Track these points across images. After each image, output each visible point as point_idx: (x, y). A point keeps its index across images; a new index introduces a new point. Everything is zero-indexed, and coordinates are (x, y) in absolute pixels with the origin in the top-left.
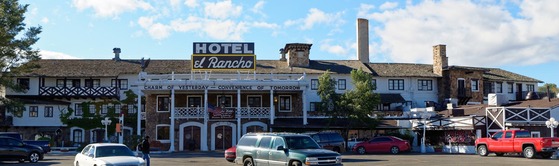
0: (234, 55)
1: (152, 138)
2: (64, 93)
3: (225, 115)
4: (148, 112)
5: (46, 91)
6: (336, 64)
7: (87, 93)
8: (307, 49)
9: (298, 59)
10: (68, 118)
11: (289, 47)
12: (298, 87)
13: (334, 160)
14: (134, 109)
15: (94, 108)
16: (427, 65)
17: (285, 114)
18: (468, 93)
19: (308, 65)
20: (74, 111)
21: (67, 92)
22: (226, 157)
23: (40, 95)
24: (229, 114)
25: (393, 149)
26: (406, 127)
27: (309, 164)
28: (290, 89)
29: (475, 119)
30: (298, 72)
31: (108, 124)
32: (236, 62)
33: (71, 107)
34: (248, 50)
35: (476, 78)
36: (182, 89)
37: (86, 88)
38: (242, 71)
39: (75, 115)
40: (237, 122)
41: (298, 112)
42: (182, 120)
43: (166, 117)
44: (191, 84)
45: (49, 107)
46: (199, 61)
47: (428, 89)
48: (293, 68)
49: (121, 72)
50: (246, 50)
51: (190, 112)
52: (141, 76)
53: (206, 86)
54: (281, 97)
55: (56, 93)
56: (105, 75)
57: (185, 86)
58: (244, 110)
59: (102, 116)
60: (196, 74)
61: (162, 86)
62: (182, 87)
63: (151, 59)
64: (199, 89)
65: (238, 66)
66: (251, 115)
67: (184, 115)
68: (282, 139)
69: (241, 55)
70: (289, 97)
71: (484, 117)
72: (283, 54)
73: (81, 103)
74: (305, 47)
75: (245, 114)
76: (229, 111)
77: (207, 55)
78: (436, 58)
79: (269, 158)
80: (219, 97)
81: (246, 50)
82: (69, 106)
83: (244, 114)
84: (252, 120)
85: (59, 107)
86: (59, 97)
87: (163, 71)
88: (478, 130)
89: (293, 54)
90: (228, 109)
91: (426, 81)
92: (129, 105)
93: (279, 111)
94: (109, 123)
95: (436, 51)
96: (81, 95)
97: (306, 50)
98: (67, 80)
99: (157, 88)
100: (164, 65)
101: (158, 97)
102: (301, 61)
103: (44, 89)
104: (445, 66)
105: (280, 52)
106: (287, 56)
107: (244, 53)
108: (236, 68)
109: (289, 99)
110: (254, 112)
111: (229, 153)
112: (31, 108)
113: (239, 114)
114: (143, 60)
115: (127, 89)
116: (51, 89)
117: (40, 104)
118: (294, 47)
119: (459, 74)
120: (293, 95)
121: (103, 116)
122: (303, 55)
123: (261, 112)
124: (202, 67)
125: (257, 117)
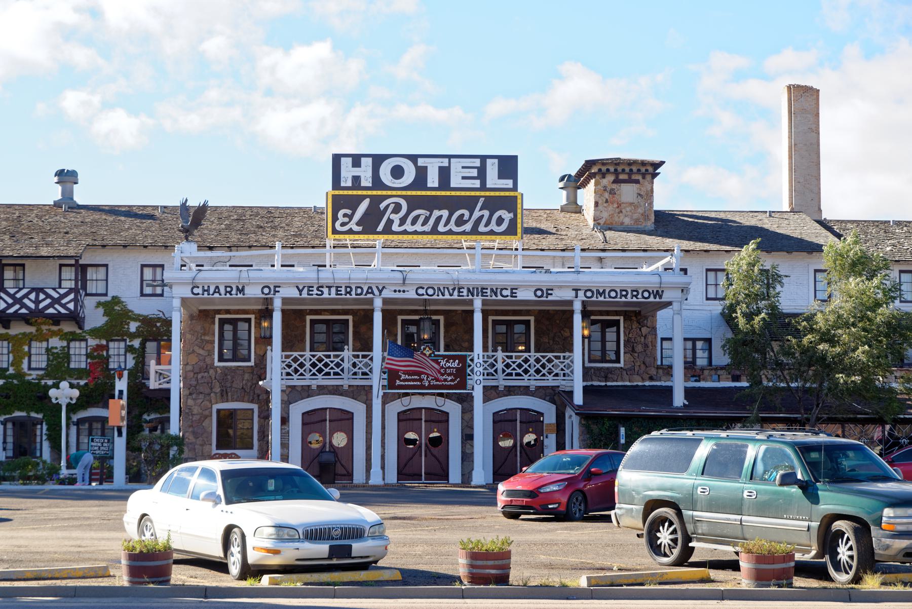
1: (202, 445)
4: (188, 364)
6: (735, 222)
14: (128, 355)
15: (5, 351)
17: (602, 374)
19: (650, 224)
22: (500, 505)
24: (448, 371)
27: (892, 529)
28: (633, 296)
30: (626, 247)
31: (68, 400)
32: (463, 215)
36: (305, 294)
38: (486, 241)
40: (473, 397)
41: (643, 367)
42: (297, 391)
43: (243, 380)
44: (334, 279)
48: (609, 234)
49: (90, 241)
50: (493, 179)
51: (526, 366)
52: (183, 255)
53: (377, 287)
59: (30, 378)
61: (243, 287)
63: (210, 204)
64: (357, 295)
65: (468, 227)
66: (507, 375)
68: (789, 451)
69: (478, 193)
70: (616, 323)
72: (571, 190)
76: (448, 365)
77: (374, 193)
79: (745, 508)
80: (403, 320)
81: (493, 179)
87: (217, 241)
92: (111, 344)
93: (252, 363)
94: (71, 399)
97: (644, 178)
98: (5, 268)
100: (213, 222)
101: (220, 319)
105: (561, 184)
106: (587, 196)
107: (488, 186)
108: (464, 233)
109: (615, 329)
110: (514, 366)
111: (510, 493)
114: (184, 206)
115: (106, 295)
118: (608, 170)
120: (627, 315)
121: (34, 377)
122: (636, 195)
123: (308, 365)
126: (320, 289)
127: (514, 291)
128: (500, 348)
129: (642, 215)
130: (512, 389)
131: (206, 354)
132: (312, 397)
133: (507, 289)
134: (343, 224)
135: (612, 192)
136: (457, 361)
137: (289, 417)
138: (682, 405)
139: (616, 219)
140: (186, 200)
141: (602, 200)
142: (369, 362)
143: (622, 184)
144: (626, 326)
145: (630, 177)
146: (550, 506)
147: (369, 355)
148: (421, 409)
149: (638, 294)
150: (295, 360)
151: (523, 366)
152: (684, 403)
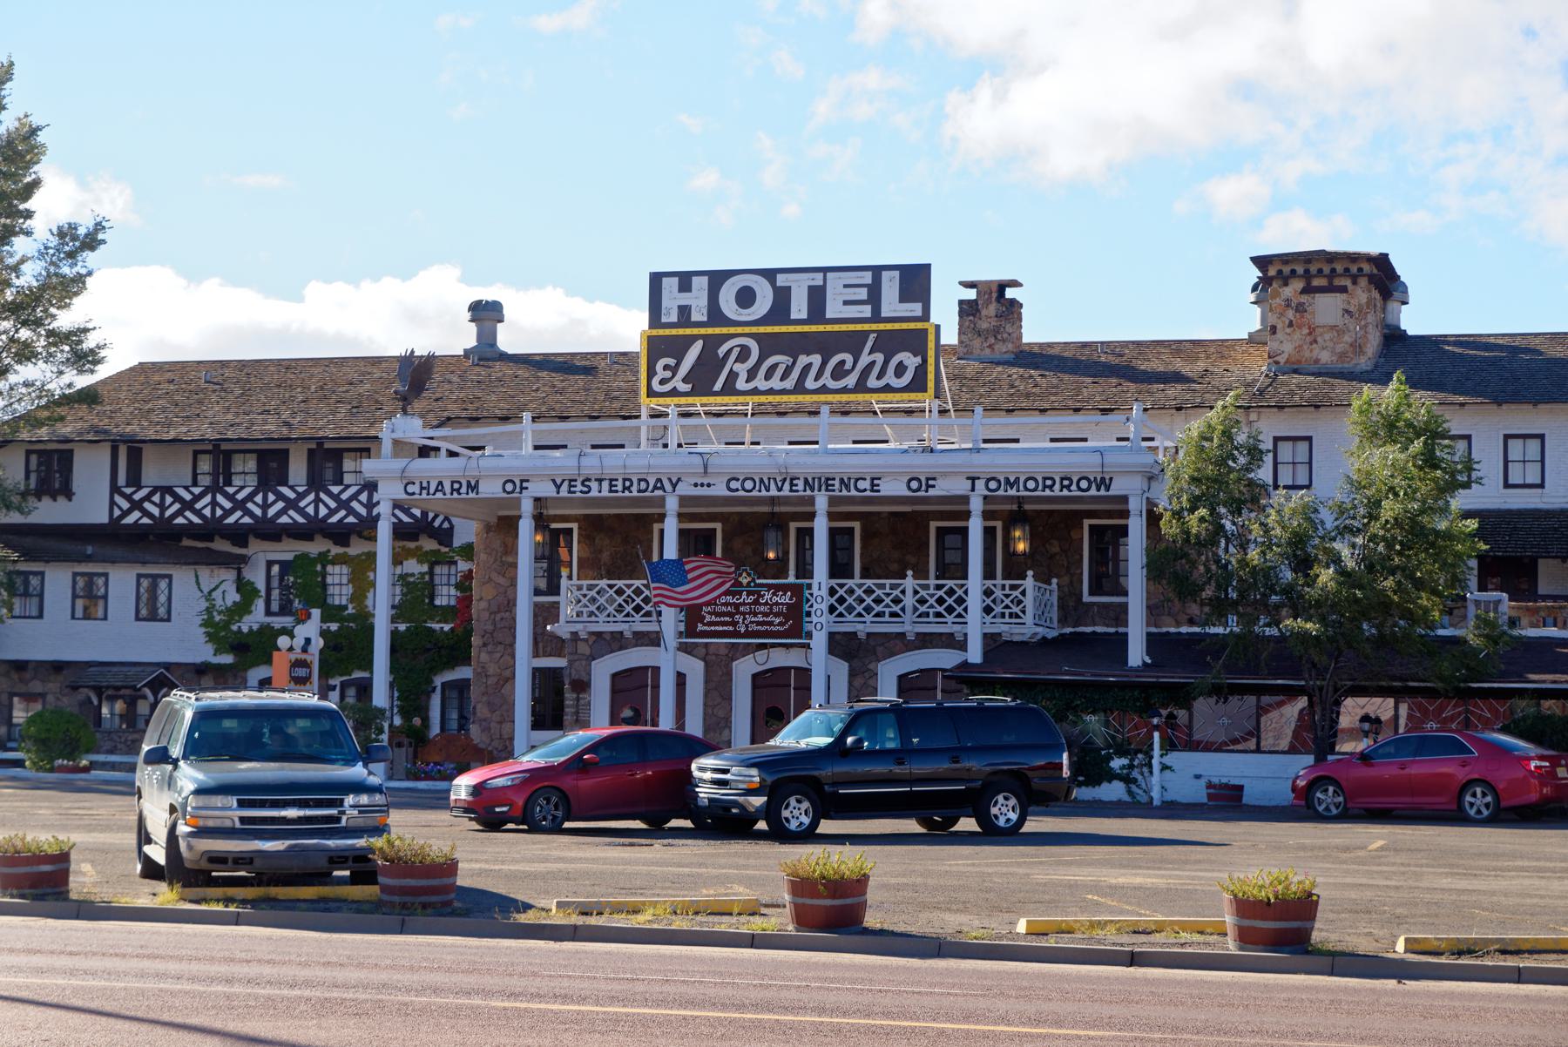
0: (836, 328)
1: (500, 723)
3: (755, 614)
4: (481, 599)
5: (136, 505)
7: (302, 512)
10: (234, 628)
12: (1103, 479)
13: (333, 812)
15: (345, 580)
20: (263, 593)
21: (222, 508)
23: (115, 522)
24: (775, 609)
25: (1319, 795)
28: (1063, 487)
32: (843, 362)
33: (248, 575)
34: (901, 301)
36: (564, 492)
37: (197, 490)
39: (268, 613)
42: (605, 639)
46: (671, 362)
50: (891, 303)
53: (670, 480)
55: (179, 513)
57: (582, 479)
58: (888, 591)
60: (759, 420)
62: (565, 487)
65: (851, 381)
67: (860, 615)
69: (866, 327)
73: (289, 557)
74: (1354, 269)
76: (776, 599)
77: (710, 331)
81: (891, 303)
82: (239, 571)
83: (931, 611)
84: (926, 641)
85: (197, 577)
86: (190, 530)
89: (1288, 306)
90: (769, 587)
93: (1086, 598)
96: (279, 521)
97: (1355, 283)
98: (345, 454)
99: (458, 491)
102: (1331, 340)
103: (128, 498)
105: (1252, 297)
110: (888, 600)
112: (81, 582)
113: (819, 613)
116: (158, 495)
118: (1293, 272)
126: (587, 483)
127: (876, 482)
128: (910, 573)
129: (1351, 345)
130: (928, 637)
131: (508, 584)
132: (626, 648)
133: (865, 479)
134: (663, 382)
135: (1300, 309)
136: (789, 593)
137: (590, 680)
138: (1140, 663)
139: (1307, 354)
141: (1283, 322)
142: (1021, 597)
143: (1317, 295)
144: (1151, 534)
145: (1331, 283)
146: (497, 810)
147: (597, 585)
149: (1071, 484)
150: (951, 592)
151: (955, 601)
152: (1144, 661)
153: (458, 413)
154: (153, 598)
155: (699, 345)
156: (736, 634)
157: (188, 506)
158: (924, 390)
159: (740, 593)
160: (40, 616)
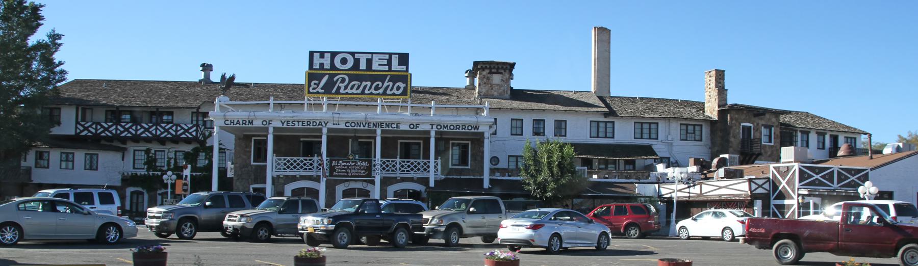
0: (376, 73)
2: (114, 132)
3: (355, 169)
5: (86, 129)
7: (150, 133)
8: (507, 71)
9: (491, 85)
11: (479, 67)
16: (697, 102)
18: (756, 147)
21: (120, 130)
23: (77, 134)
24: (362, 168)
26: (649, 196)
29: (752, 183)
32: (378, 85)
34: (399, 65)
35: (769, 124)
45: (91, 155)
47: (696, 139)
50: (395, 66)
53: (324, 122)
54: (453, 144)
56: (180, 105)
57: (291, 121)
61: (252, 121)
65: (381, 91)
66: (402, 171)
67: (415, 171)
69: (387, 73)
71: (767, 180)
74: (505, 67)
75: (392, 171)
76: (362, 164)
77: (331, 72)
78: (710, 90)
81: (395, 66)
84: (404, 180)
86: (107, 138)
88: (758, 201)
89: (484, 77)
91: (692, 127)
95: (710, 78)
97: (505, 71)
103: (83, 126)
104: (723, 103)
105: (466, 75)
110: (406, 166)
117: (76, 148)
118: (486, 67)
119: (743, 117)
124: (322, 91)
125: (412, 174)
133: (394, 124)
134: (314, 89)
139: (490, 93)
140: (225, 74)
148: (356, 188)
153: (207, 100)
154: (91, 162)
155: (327, 76)
156: (348, 176)
157: (106, 129)
158: (407, 95)
159: (349, 162)
160: (48, 167)
